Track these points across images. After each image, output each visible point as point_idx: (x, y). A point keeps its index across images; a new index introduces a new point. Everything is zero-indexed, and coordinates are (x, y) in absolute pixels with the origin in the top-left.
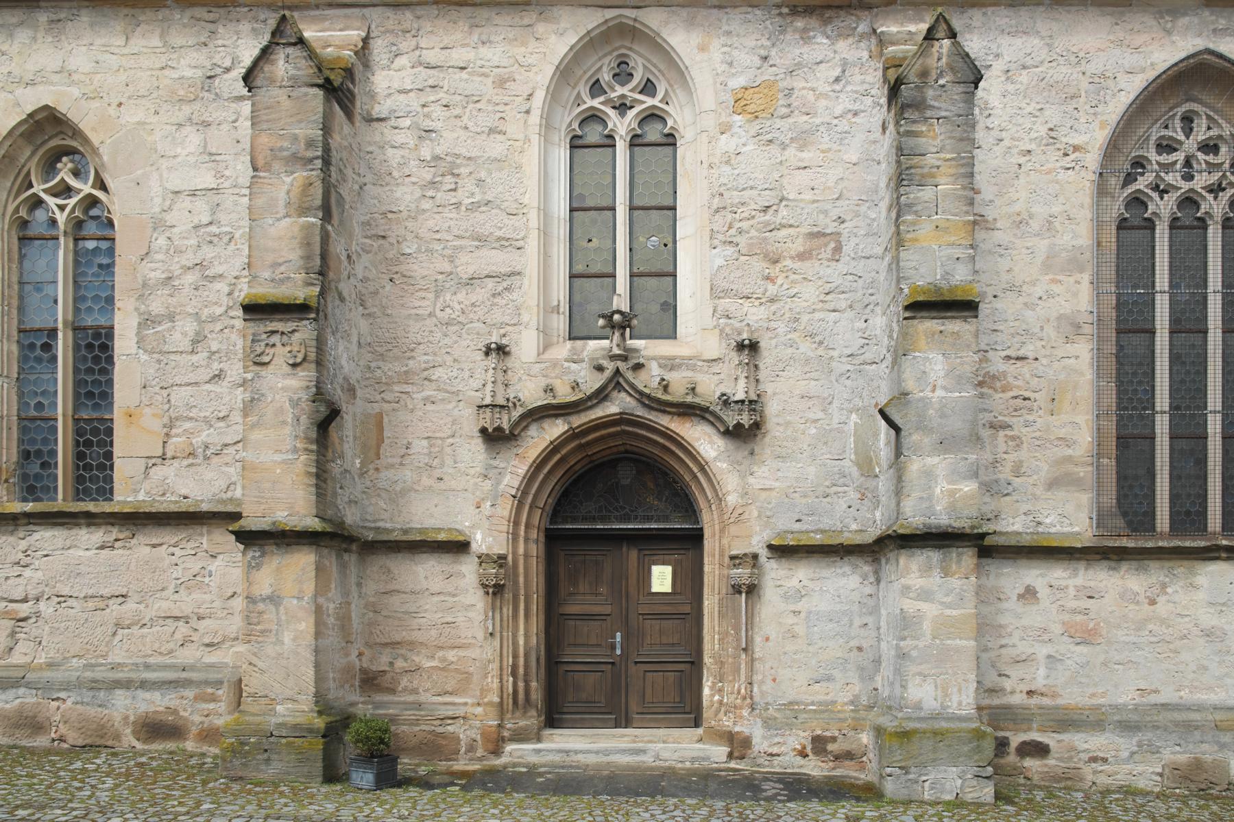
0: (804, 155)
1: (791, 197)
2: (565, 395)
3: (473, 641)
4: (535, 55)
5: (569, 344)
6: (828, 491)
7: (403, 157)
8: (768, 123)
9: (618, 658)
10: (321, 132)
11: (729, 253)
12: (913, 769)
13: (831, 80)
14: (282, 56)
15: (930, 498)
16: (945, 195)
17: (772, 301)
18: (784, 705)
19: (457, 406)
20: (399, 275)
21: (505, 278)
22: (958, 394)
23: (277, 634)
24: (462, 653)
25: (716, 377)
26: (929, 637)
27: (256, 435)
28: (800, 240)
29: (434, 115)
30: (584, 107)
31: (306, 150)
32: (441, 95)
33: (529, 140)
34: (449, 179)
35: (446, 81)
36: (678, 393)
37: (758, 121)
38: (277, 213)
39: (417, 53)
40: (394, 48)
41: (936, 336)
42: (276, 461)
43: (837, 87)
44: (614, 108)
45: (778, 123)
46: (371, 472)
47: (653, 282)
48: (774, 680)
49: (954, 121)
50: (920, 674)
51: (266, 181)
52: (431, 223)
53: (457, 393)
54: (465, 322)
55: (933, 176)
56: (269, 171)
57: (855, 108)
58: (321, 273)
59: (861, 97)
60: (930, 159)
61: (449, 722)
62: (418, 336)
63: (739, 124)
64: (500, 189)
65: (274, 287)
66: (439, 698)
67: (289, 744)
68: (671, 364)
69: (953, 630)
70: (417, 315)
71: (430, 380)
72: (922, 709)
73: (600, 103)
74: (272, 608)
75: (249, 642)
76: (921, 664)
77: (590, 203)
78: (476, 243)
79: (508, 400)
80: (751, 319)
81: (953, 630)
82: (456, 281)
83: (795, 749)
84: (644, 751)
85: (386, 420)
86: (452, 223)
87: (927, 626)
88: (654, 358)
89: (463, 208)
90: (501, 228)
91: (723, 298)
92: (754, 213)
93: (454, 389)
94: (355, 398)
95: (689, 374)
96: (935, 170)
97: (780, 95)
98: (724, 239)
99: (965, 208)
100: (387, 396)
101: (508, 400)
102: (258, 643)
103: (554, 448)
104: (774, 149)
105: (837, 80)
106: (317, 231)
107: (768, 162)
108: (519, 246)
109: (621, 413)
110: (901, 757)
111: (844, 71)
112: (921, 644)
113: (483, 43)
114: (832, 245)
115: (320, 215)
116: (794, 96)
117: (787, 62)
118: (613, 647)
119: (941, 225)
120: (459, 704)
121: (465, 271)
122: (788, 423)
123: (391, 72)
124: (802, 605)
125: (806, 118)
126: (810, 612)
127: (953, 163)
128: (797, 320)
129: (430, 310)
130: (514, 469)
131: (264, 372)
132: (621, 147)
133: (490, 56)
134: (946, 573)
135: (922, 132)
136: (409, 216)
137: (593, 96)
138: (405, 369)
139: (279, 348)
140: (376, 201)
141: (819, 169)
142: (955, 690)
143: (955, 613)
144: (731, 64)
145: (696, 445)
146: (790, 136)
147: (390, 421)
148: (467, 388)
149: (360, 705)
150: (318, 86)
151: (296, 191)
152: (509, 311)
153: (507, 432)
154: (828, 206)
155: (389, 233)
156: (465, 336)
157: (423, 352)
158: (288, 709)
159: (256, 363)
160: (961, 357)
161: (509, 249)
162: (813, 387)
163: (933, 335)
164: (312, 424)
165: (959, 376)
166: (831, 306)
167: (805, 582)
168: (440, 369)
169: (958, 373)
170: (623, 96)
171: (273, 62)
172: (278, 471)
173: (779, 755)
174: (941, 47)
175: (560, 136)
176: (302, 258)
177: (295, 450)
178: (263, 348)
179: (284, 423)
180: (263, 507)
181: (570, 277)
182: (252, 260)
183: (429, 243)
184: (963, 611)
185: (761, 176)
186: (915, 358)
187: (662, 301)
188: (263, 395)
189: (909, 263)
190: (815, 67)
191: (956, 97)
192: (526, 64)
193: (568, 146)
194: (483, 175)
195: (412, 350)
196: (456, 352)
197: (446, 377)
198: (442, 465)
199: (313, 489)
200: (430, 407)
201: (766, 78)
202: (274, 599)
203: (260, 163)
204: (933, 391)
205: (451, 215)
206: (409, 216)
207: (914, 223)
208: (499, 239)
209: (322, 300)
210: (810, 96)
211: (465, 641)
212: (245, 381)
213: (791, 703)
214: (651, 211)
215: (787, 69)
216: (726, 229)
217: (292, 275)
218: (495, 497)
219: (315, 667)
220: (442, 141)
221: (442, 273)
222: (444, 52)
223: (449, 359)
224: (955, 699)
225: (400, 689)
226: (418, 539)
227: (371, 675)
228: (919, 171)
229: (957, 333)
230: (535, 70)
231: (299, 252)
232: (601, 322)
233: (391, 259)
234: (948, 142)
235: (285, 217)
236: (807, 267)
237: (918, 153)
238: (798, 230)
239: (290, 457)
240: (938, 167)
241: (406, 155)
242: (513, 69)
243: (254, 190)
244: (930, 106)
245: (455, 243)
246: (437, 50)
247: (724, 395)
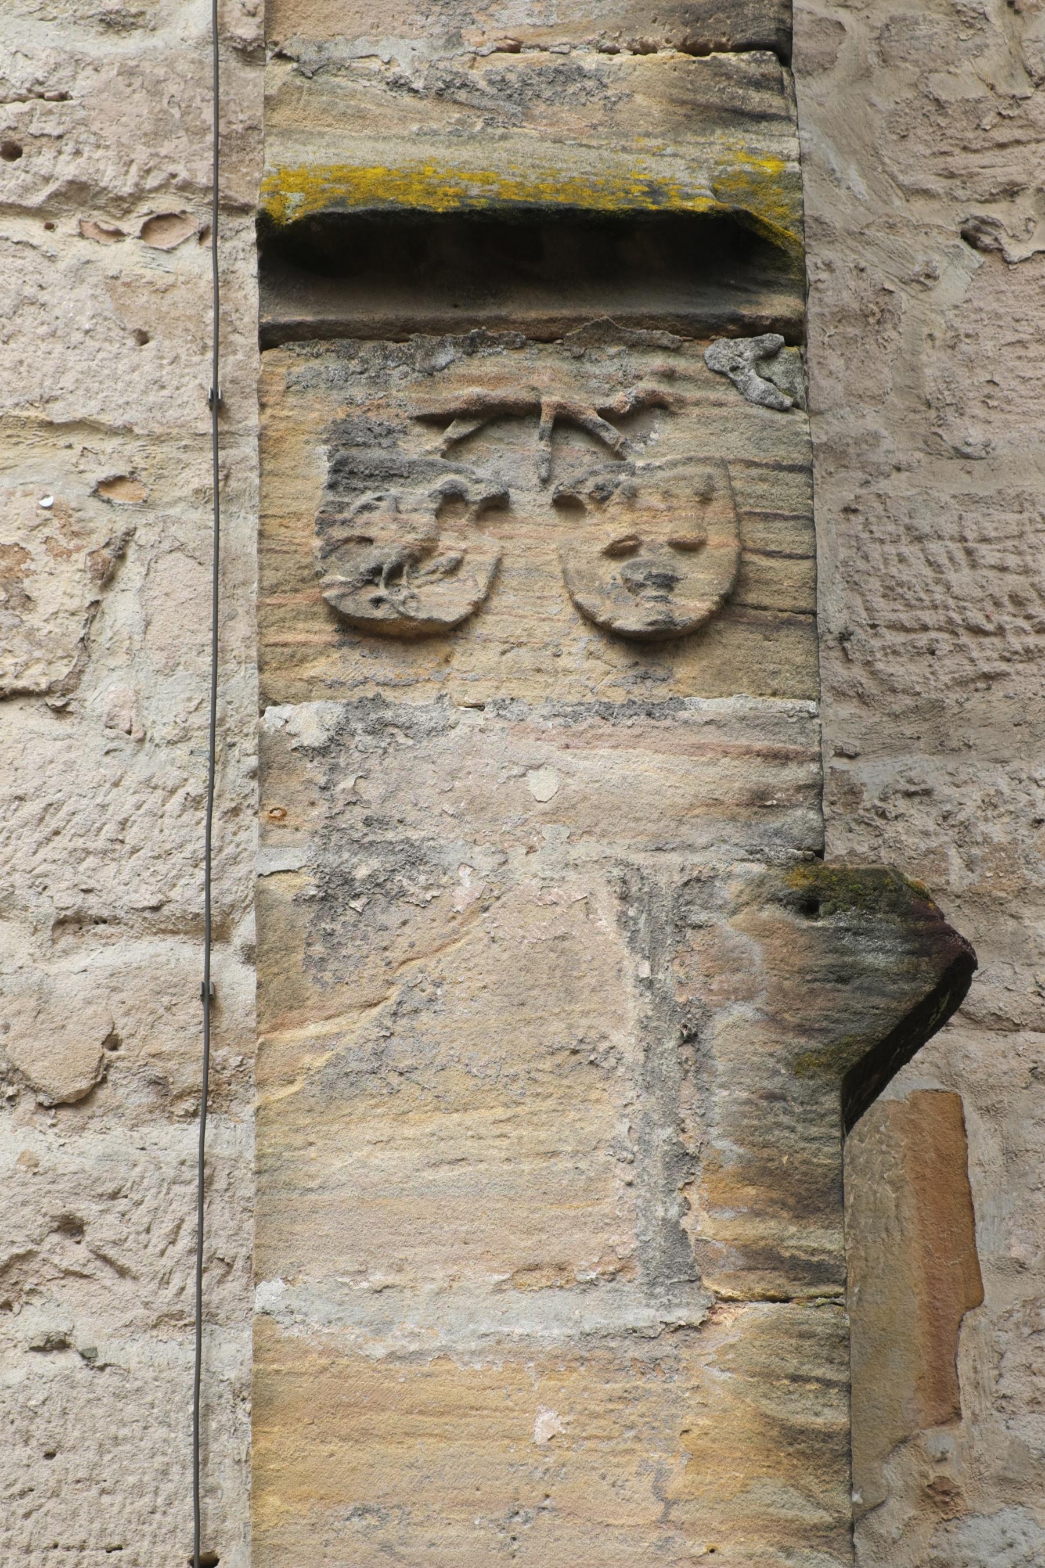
65: (459, 134)
147: (1011, 1154)
164: (799, 1066)
178: (424, 520)
188: (415, 859)
217: (591, 61)
233: (972, 109)
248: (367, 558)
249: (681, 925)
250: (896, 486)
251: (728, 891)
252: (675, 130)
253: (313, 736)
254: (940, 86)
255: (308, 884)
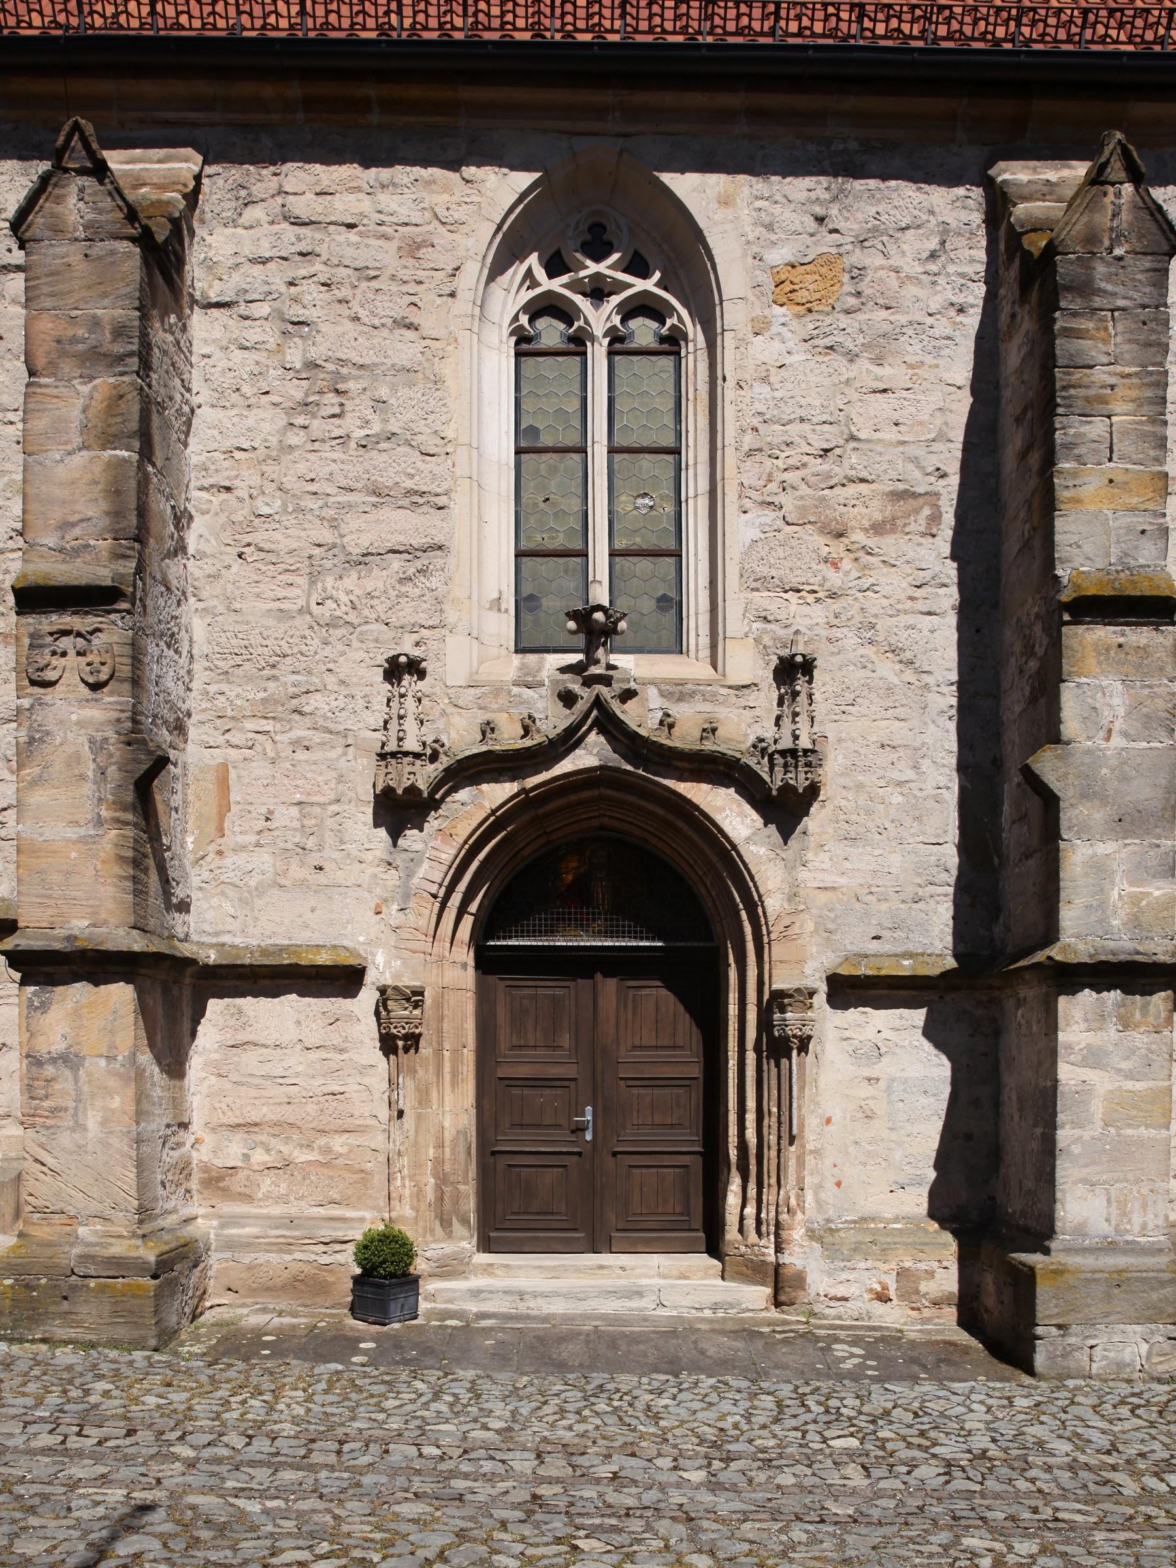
0: (885, 371)
1: (862, 435)
2: (509, 738)
3: (374, 1122)
4: (465, 206)
5: (517, 659)
6: (920, 892)
7: (257, 363)
8: (828, 320)
9: (589, 1147)
10: (138, 313)
11: (768, 520)
12: (1074, 1328)
13: (926, 255)
14: (74, 189)
15: (1102, 905)
16: (1125, 433)
17: (833, 596)
18: (855, 1222)
19: (345, 754)
20: (252, 548)
21: (418, 554)
22: (1145, 744)
23: (75, 1115)
24: (353, 1139)
25: (747, 712)
26: (1099, 1123)
27: (37, 797)
28: (875, 504)
29: (306, 299)
30: (538, 291)
31: (113, 341)
32: (318, 267)
33: (456, 340)
34: (331, 398)
35: (326, 245)
36: (685, 738)
37: (810, 317)
38: (66, 443)
39: (279, 200)
40: (243, 193)
41: (1112, 653)
42: (68, 840)
43: (933, 267)
44: (584, 295)
45: (844, 321)
46: (211, 856)
47: (644, 564)
48: (838, 1184)
49: (1137, 315)
50: (1085, 1181)
51: (47, 391)
52: (302, 468)
53: (345, 733)
54: (356, 622)
55: (1103, 400)
56: (54, 375)
57: (961, 301)
58: (137, 539)
59: (970, 283)
60: (1100, 375)
61: (338, 1247)
62: (283, 643)
63: (783, 320)
64: (410, 415)
65: (64, 561)
66: (320, 1209)
67: (102, 1289)
68: (679, 691)
69: (1134, 1112)
70: (281, 610)
71: (300, 713)
72: (1085, 1235)
73: (562, 286)
74: (68, 1073)
75: (33, 1126)
76: (1086, 1166)
77: (546, 440)
78: (374, 499)
79: (424, 744)
80: (801, 624)
81: (1134, 1112)
82: (342, 557)
83: (871, 1290)
84: (639, 1294)
85: (233, 774)
86: (334, 467)
87: (1097, 1108)
88: (653, 682)
89: (353, 445)
90: (412, 476)
91: (758, 590)
92: (806, 459)
93: (341, 728)
94: (186, 741)
95: (707, 707)
96: (1109, 391)
97: (846, 278)
98: (760, 499)
99: (1152, 453)
100: (236, 738)
101: (424, 744)
102: (48, 1128)
103: (498, 822)
104: (838, 361)
105: (933, 256)
106: (132, 471)
107: (827, 382)
108: (440, 504)
109: (601, 768)
110: (1056, 1311)
111: (943, 243)
112: (1087, 1135)
113: (383, 186)
114: (927, 511)
115: (137, 444)
116: (867, 279)
117: (856, 226)
118: (580, 1129)
119: (1119, 478)
120: (352, 1219)
121: (357, 543)
122: (860, 786)
123: (239, 231)
124: (883, 1068)
125: (884, 314)
126: (893, 1080)
127: (1135, 381)
128: (873, 626)
129: (301, 602)
130: (434, 853)
131: (48, 695)
132: (598, 353)
133: (394, 207)
134: (1126, 1024)
135: (1088, 330)
136: (269, 457)
137: (551, 276)
138: (262, 695)
139: (72, 659)
140: (216, 432)
141: (905, 394)
142: (1137, 1205)
143: (1139, 1086)
144: (769, 227)
145: (718, 818)
146: (861, 340)
148: (360, 725)
149: (199, 1220)
150: (133, 239)
151: (98, 406)
152: (425, 606)
153: (425, 795)
154: (921, 452)
155: (237, 483)
156: (356, 644)
157: (291, 668)
158: (96, 1232)
159: (33, 683)
160: (1150, 686)
161: (425, 509)
162: (898, 732)
163: (1107, 650)
165: (1147, 716)
166: (921, 606)
167: (887, 1033)
168: (318, 696)
169: (1145, 710)
170: (597, 276)
171: (60, 200)
172: (74, 855)
173: (846, 1299)
174: (1118, 195)
175: (501, 335)
176: (107, 513)
177: (99, 822)
179: (82, 777)
180: (50, 912)
181: (516, 556)
182: (28, 517)
183: (299, 498)
184: (1151, 1084)
185: (817, 403)
186: (1079, 685)
187: (660, 593)
188: (48, 733)
189: (1068, 536)
190: (898, 235)
191: (1138, 277)
192: (450, 220)
193: (512, 353)
194: (383, 392)
195: (274, 666)
196: (344, 669)
197: (327, 708)
198: (320, 847)
199: (129, 884)
200: (302, 755)
201: (825, 249)
202: (69, 1060)
203: (41, 362)
204: (1108, 739)
205: (335, 456)
206: (269, 457)
207: (1075, 474)
208: (409, 492)
209: (139, 583)
210: (893, 281)
211: (358, 1122)
212: (19, 710)
213: (864, 1219)
214: (642, 456)
215: (856, 237)
216: (762, 483)
217: (92, 542)
218: (406, 896)
219: (137, 1167)
220: (319, 338)
221: (319, 546)
222: (320, 199)
223: (331, 680)
224: (1137, 1219)
225: (260, 1195)
226: (286, 962)
227: (214, 1174)
228: (1082, 392)
229: (1144, 649)
230: (464, 229)
231: (104, 505)
232: (572, 625)
233: (241, 523)
234: (1127, 347)
235: (80, 449)
236: (889, 545)
237: (1081, 363)
238: (873, 486)
239: (92, 832)
240: (1112, 387)
241: (263, 360)
242: (430, 228)
243: (30, 406)
244: (1099, 290)
245: (339, 499)
246: (310, 196)
247: (762, 740)
248: (37, 666)
249: (102, 748)
250: (220, 618)
251: (112, 741)
252: (110, 560)
253: (27, 706)
254: (234, 518)
255: (26, 739)
